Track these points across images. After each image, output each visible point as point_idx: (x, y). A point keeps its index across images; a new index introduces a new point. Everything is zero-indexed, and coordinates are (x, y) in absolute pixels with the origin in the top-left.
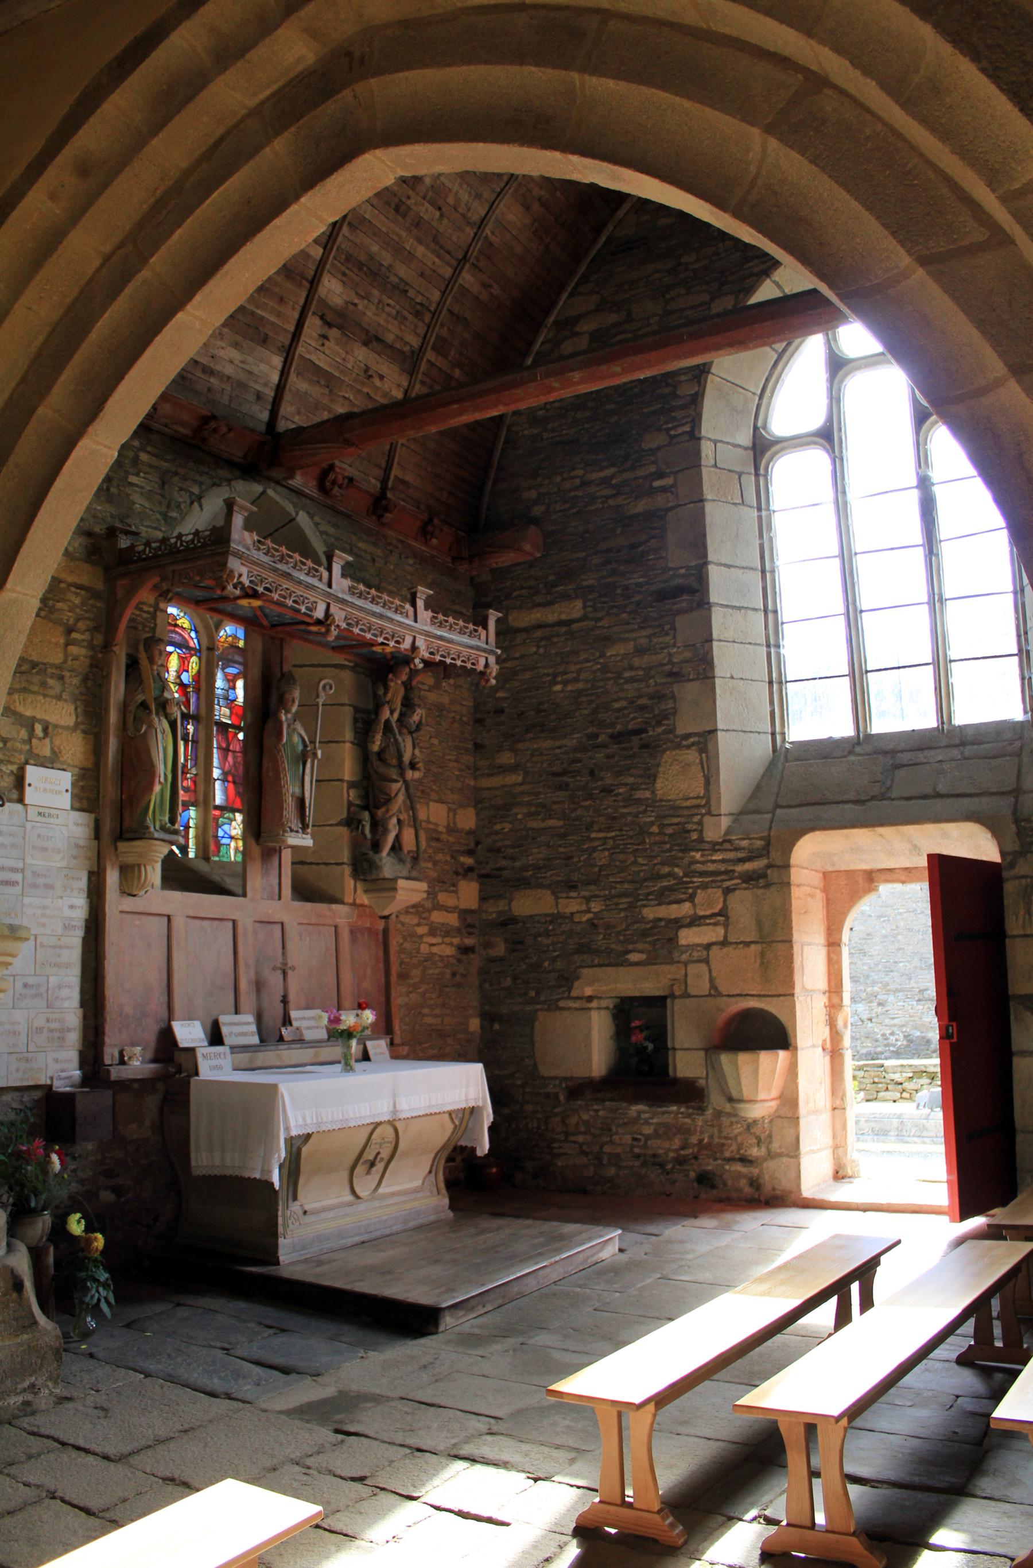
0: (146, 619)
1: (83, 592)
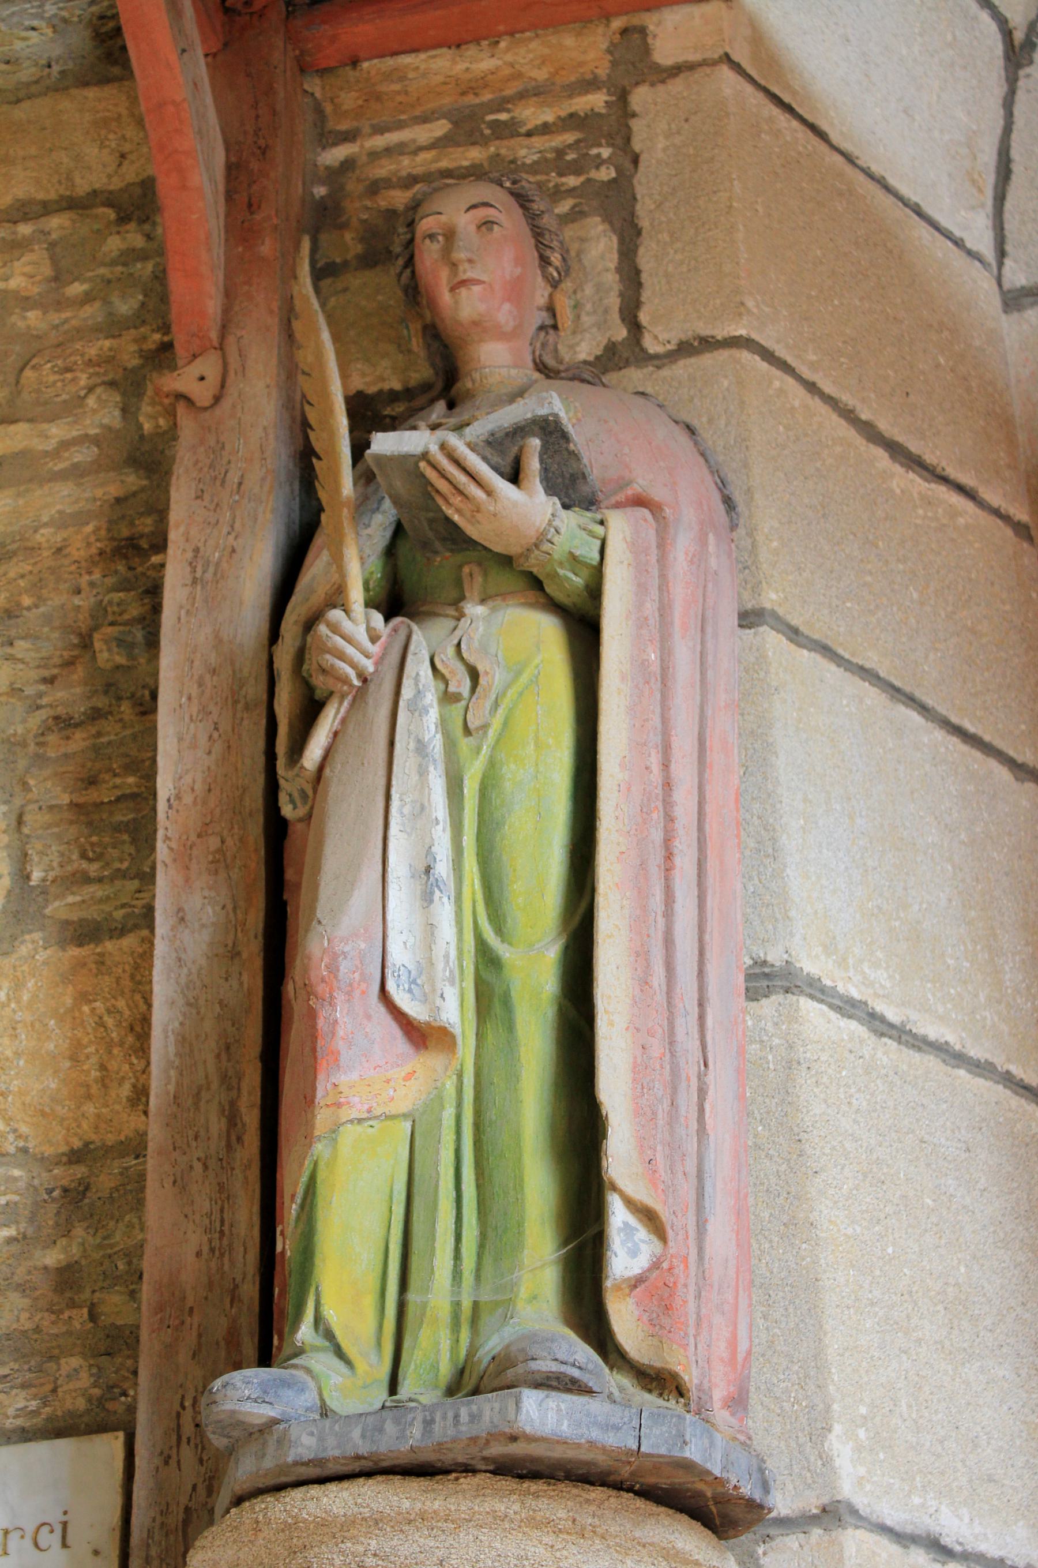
0: (559, 163)
1: (57, 223)
